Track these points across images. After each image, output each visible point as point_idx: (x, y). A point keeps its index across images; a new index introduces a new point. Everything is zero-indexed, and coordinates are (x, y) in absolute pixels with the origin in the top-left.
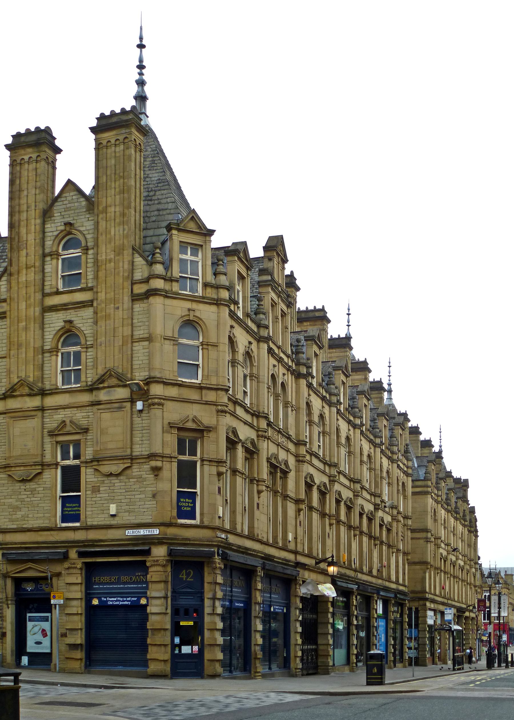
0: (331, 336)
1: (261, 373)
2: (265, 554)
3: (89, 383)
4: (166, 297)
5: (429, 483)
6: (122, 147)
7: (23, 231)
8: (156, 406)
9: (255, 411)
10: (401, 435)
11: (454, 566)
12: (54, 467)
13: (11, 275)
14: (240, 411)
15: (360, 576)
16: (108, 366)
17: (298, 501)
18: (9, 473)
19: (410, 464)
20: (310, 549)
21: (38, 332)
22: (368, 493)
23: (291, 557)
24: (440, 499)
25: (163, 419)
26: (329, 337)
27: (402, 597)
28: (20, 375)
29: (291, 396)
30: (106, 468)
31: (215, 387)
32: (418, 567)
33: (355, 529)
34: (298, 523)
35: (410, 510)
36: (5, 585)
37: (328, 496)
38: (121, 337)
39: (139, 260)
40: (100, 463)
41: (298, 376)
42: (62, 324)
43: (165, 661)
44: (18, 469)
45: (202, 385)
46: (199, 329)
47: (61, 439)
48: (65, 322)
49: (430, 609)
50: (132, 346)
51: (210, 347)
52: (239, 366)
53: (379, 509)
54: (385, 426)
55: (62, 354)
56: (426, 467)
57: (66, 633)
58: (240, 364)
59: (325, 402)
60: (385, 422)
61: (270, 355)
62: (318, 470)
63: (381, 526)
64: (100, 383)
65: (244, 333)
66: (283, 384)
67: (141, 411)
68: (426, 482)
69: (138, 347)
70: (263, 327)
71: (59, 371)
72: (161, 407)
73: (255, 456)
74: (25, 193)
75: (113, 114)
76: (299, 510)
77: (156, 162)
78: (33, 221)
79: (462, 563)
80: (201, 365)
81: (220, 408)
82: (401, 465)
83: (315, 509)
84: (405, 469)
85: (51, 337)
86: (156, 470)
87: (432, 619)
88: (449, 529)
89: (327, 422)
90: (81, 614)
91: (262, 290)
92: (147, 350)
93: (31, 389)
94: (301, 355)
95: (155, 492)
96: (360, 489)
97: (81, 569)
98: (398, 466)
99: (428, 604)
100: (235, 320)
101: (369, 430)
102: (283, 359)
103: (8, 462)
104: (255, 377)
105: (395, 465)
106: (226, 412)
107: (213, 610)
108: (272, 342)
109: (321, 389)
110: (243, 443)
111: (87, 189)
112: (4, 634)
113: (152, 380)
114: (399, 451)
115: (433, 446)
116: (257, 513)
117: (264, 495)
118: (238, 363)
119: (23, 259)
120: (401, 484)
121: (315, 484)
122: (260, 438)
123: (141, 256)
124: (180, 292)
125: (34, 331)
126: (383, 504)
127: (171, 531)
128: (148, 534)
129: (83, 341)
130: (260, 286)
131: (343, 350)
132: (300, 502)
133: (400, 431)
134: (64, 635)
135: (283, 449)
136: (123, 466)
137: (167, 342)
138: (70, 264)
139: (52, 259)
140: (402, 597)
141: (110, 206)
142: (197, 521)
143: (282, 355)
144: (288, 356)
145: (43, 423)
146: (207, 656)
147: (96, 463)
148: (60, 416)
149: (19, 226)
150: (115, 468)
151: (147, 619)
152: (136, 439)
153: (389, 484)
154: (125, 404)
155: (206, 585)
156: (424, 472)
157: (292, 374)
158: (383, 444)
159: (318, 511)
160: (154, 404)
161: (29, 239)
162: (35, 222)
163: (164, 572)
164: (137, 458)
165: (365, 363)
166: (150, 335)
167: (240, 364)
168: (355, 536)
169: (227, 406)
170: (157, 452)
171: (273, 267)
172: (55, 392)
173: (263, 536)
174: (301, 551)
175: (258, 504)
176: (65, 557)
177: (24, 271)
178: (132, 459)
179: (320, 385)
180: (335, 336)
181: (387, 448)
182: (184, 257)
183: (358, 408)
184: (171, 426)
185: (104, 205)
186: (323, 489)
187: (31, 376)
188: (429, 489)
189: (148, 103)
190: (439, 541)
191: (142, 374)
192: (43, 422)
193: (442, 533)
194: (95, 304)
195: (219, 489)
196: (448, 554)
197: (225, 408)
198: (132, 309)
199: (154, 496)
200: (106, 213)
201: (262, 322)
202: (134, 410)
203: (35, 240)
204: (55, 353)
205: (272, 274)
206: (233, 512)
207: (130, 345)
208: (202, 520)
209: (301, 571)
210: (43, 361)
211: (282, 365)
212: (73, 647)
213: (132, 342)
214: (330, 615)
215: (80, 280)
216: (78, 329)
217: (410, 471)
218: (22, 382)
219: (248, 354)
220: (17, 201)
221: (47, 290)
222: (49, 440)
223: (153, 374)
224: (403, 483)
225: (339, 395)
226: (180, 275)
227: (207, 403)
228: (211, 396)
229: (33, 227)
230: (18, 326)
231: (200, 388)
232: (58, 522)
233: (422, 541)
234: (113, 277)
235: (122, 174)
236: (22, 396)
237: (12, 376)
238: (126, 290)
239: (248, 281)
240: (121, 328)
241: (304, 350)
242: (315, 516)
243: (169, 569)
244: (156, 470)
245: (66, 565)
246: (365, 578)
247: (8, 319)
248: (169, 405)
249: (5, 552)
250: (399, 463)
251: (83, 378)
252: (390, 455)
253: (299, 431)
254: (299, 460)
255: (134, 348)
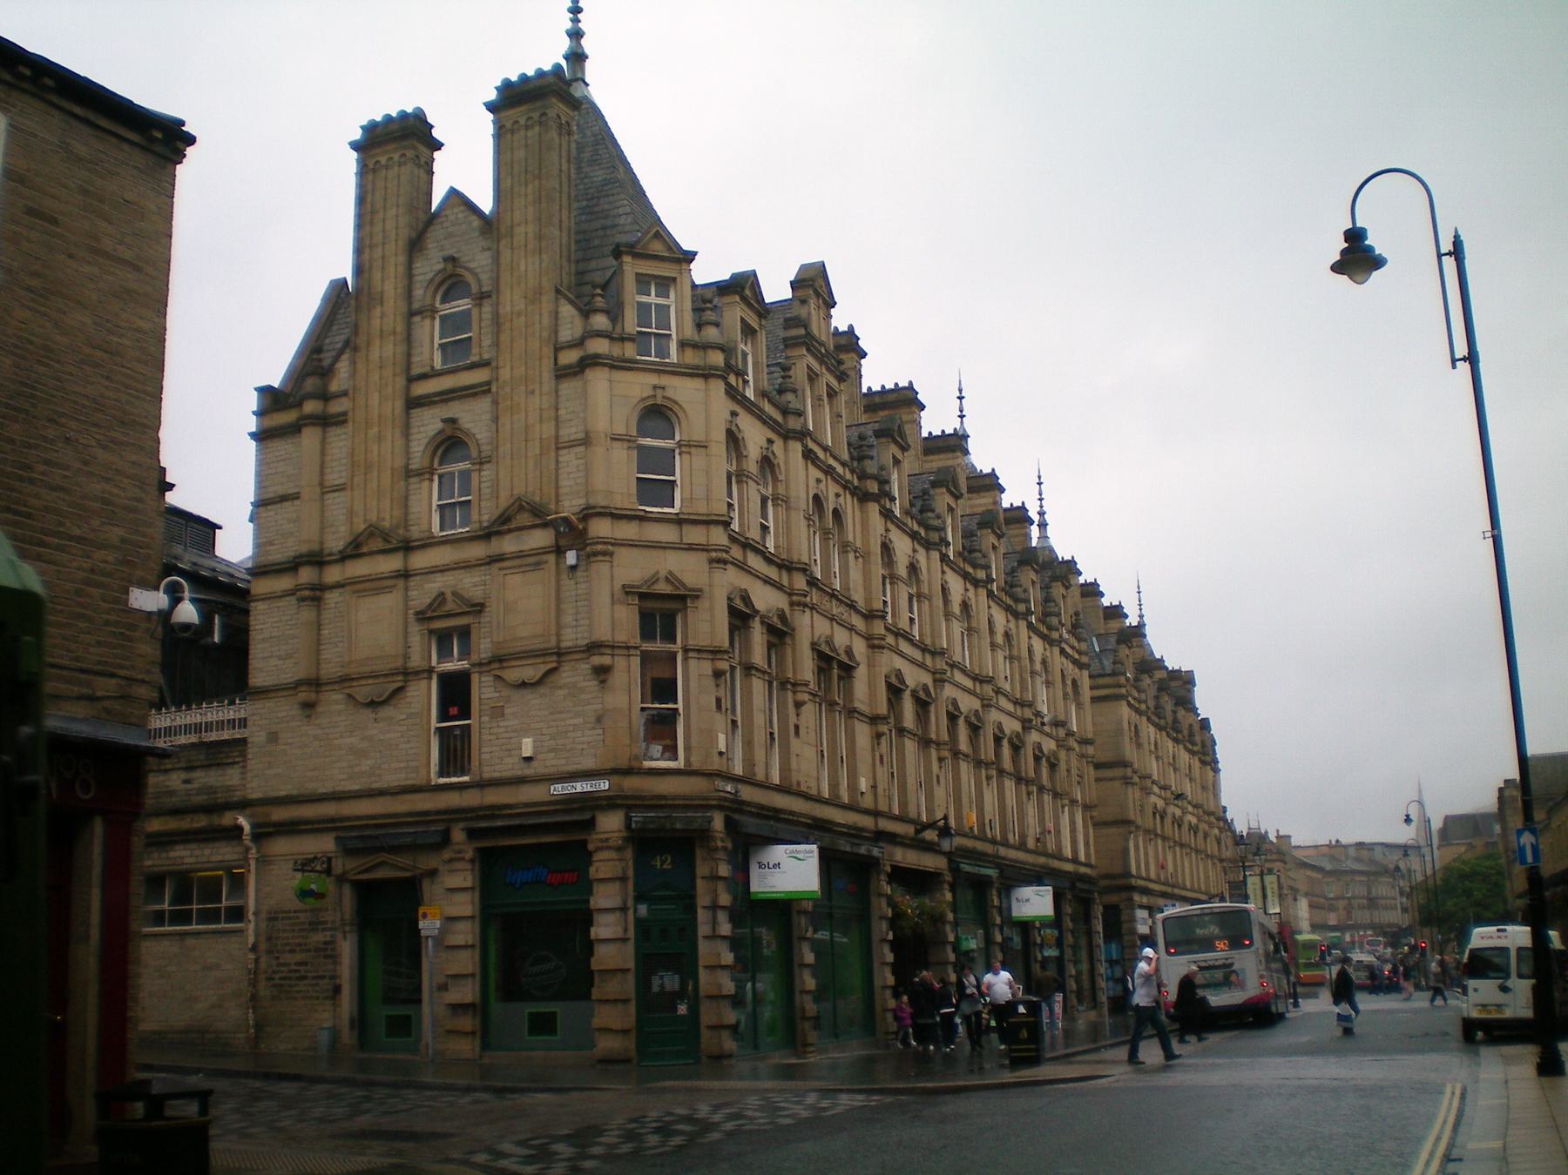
0: (869, 388)
1: (793, 494)
2: (815, 819)
3: (485, 524)
4: (612, 367)
5: (1122, 680)
6: (537, 129)
7: (377, 275)
8: (600, 558)
9: (783, 560)
10: (1063, 596)
11: (1180, 826)
12: (425, 675)
13: (356, 349)
14: (754, 561)
15: (1003, 851)
16: (515, 492)
17: (874, 720)
18: (348, 691)
19: (1083, 646)
20: (903, 804)
21: (400, 442)
22: (1009, 700)
23: (866, 822)
24: (1143, 707)
25: (612, 580)
26: (864, 390)
27: (1086, 887)
28: (368, 517)
29: (853, 532)
30: (515, 674)
31: (704, 518)
32: (1113, 830)
33: (988, 765)
34: (878, 757)
35: (1090, 728)
36: (341, 896)
37: (932, 708)
38: (537, 443)
39: (567, 310)
40: (505, 664)
41: (864, 497)
42: (440, 425)
43: (625, 1032)
44: (363, 682)
45: (681, 516)
46: (674, 419)
47: (438, 625)
48: (443, 421)
49: (1142, 907)
50: (557, 456)
51: (693, 450)
52: (749, 480)
53: (1031, 728)
54: (1033, 582)
55: (441, 477)
56: (1115, 651)
57: (447, 984)
58: (751, 478)
59: (919, 543)
60: (1033, 575)
61: (809, 464)
62: (912, 661)
63: (1037, 759)
64: (504, 523)
65: (758, 424)
66: (836, 513)
67: (573, 568)
68: (1116, 678)
69: (567, 457)
70: (793, 413)
71: (434, 507)
72: (607, 558)
73: (788, 640)
74: (381, 215)
75: (524, 79)
76: (879, 736)
77: (600, 152)
78: (392, 260)
79: (1194, 820)
80: (678, 483)
81: (714, 554)
82: (1069, 650)
83: (908, 732)
84: (1077, 656)
85: (422, 448)
86: (602, 672)
87: (1145, 923)
88: (1166, 760)
89: (924, 575)
90: (472, 946)
91: (789, 353)
92: (583, 461)
93: (386, 540)
94: (867, 462)
95: (601, 712)
96: (993, 694)
97: (472, 861)
98: (1063, 651)
99: (1137, 897)
100: (739, 402)
101: (1003, 590)
102: (834, 469)
103: (346, 671)
104: (782, 500)
105: (1056, 650)
106: (725, 562)
107: (714, 929)
108: (811, 439)
109: (909, 519)
110: (762, 617)
111: (486, 203)
112: (337, 990)
113: (591, 511)
114: (1063, 625)
115: (1126, 616)
116: (795, 744)
117: (809, 710)
118: (747, 477)
119: (376, 322)
120: (1069, 682)
121: (907, 687)
122: (796, 608)
123: (571, 302)
124: (638, 357)
125: (393, 441)
126: (1039, 720)
127: (632, 784)
128: (589, 790)
129: (474, 454)
130: (786, 346)
131: (950, 455)
132: (879, 721)
133: (1062, 590)
134: (443, 988)
135: (841, 625)
136: (543, 668)
137: (617, 444)
138: (454, 323)
139: (423, 318)
140: (1086, 887)
141: (519, 225)
142: (679, 764)
143: (831, 462)
144: (844, 464)
145: (406, 599)
146: (707, 1016)
147: (496, 665)
148: (436, 584)
149: (371, 268)
150: (529, 672)
151: (591, 953)
152: (568, 619)
153: (1048, 684)
154: (545, 557)
155: (699, 882)
156: (1111, 660)
157: (853, 494)
158: (1032, 613)
159: (915, 735)
160: (595, 554)
161: (386, 288)
162: (397, 261)
163: (620, 860)
164: (569, 652)
165: (993, 475)
166: (587, 433)
167: (751, 478)
168: (989, 778)
169: (727, 552)
170: (603, 639)
171: (809, 314)
172: (429, 543)
173: (809, 785)
174: (886, 810)
175: (797, 727)
176: (445, 840)
177: (377, 342)
178: (560, 654)
179: (907, 513)
180: (876, 388)
181: (1038, 620)
182: (644, 299)
183: (980, 551)
184: (628, 590)
185: (509, 224)
186: (922, 695)
187: (387, 515)
188: (1123, 691)
189: (588, 64)
190: (1148, 782)
191: (574, 503)
192: (407, 596)
193: (1153, 767)
194: (494, 389)
195: (718, 701)
196: (1166, 804)
197: (724, 555)
198: (557, 391)
199: (599, 720)
200: (512, 237)
201: (791, 406)
202: (562, 566)
203: (396, 289)
204: (427, 476)
205: (806, 327)
206: (748, 744)
207: (553, 454)
208: (687, 760)
209: (888, 848)
210: (408, 490)
211: (834, 479)
212: (457, 1008)
213: (558, 449)
214: (948, 928)
215: (469, 350)
216: (467, 432)
217: (1085, 659)
218: (373, 531)
219: (767, 462)
220: (367, 228)
221: (416, 371)
222: (417, 629)
223: (592, 502)
224: (1074, 682)
225: (944, 529)
226: (639, 329)
227: (691, 548)
228: (695, 535)
229: (392, 269)
230: (366, 434)
231: (679, 521)
232: (432, 775)
233: (1117, 784)
234: (523, 341)
235: (537, 172)
236: (371, 553)
237: (355, 520)
238: (545, 362)
239: (762, 338)
240: (537, 426)
241: (874, 453)
242: (910, 746)
243: (629, 854)
244: (602, 672)
245: (447, 855)
246: (1013, 854)
247: (350, 424)
248: (623, 554)
249: (341, 834)
250: (1064, 645)
251: (475, 516)
252: (1045, 631)
253: (870, 593)
254: (874, 645)
255: (561, 459)
